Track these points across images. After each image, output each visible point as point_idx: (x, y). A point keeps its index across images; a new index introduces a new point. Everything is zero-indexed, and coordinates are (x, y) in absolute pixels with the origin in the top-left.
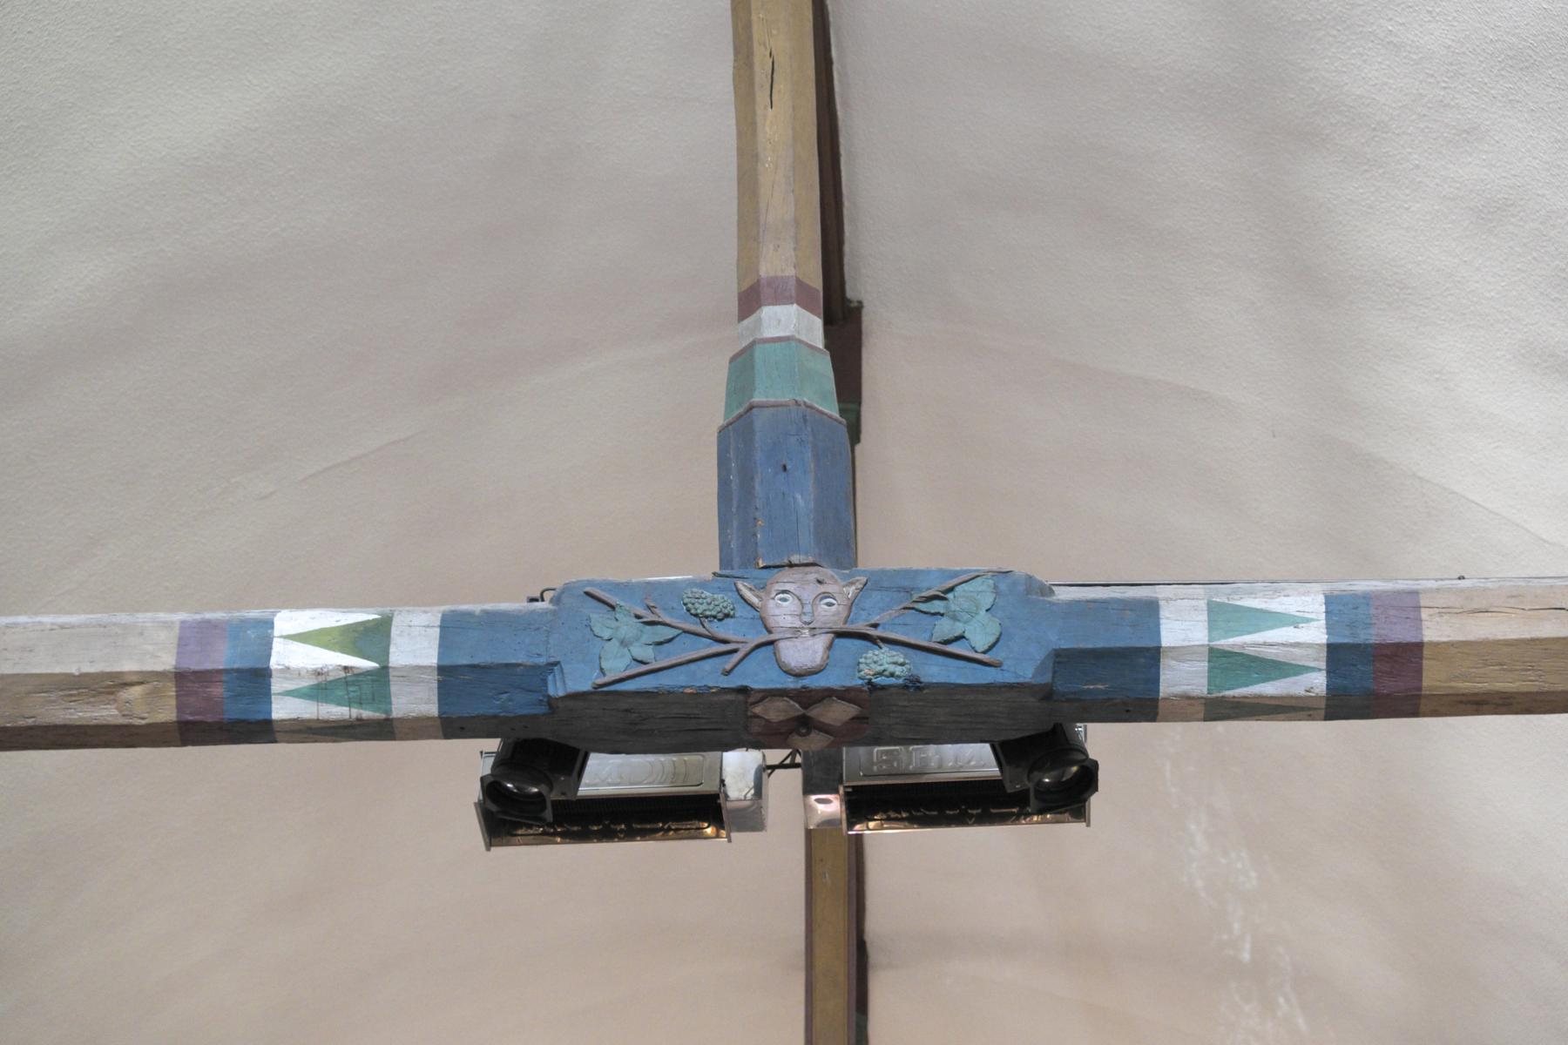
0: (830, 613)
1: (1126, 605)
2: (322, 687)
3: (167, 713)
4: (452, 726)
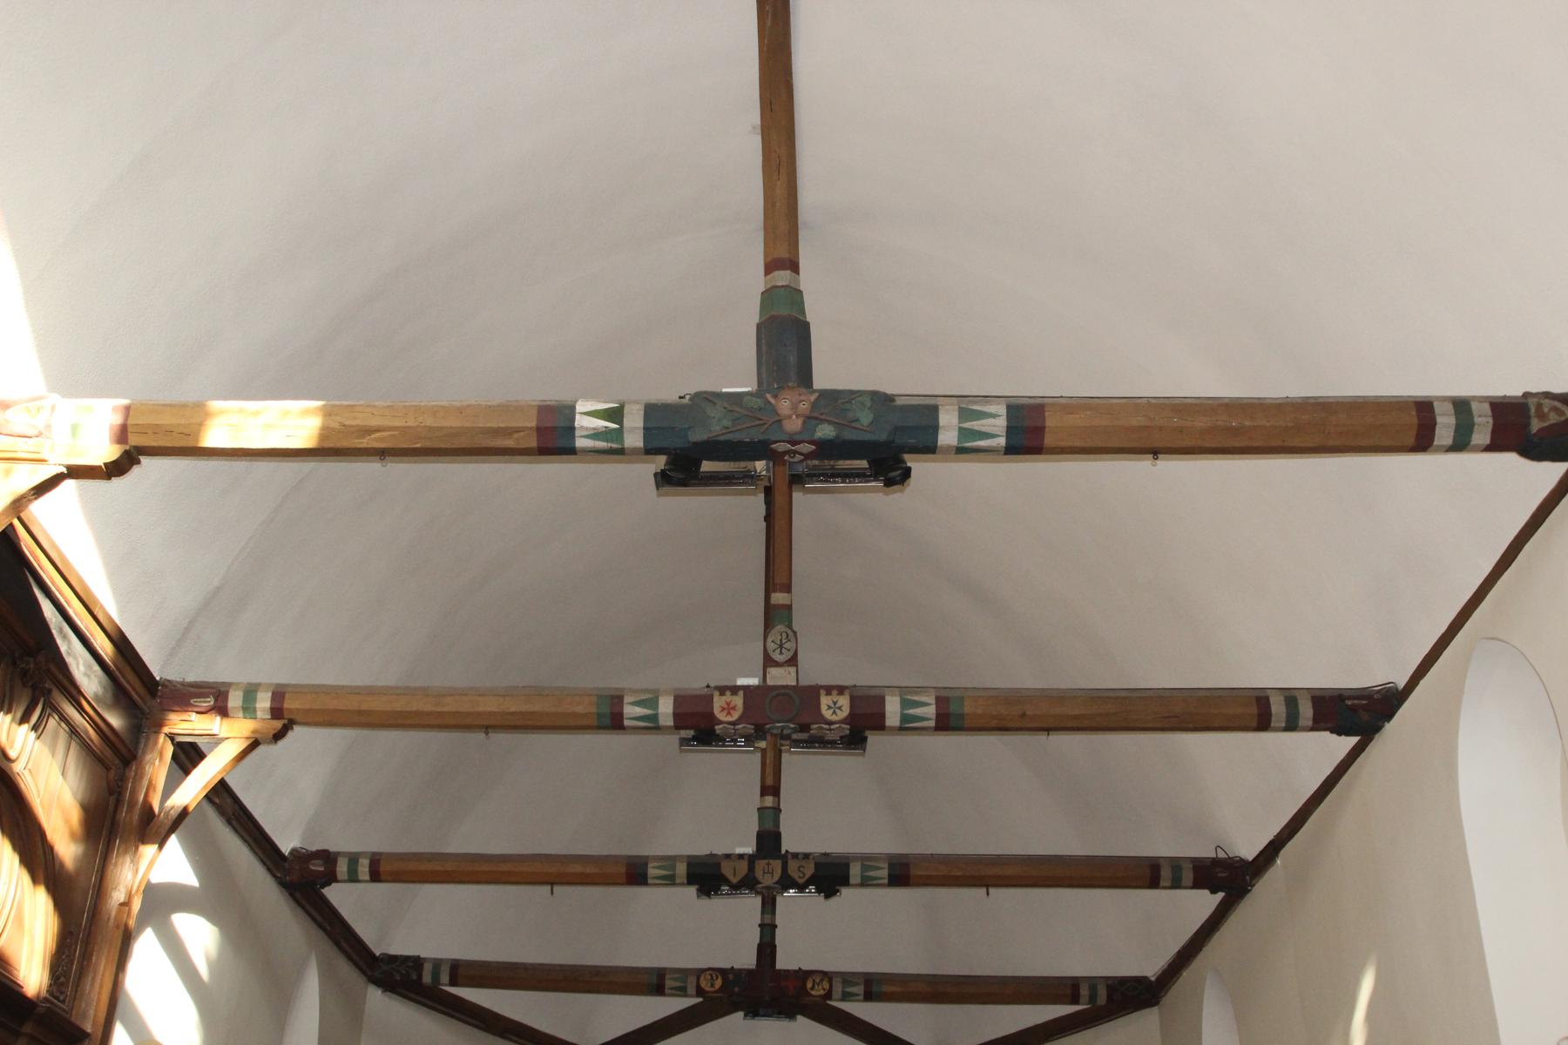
0: (804, 407)
1: (927, 407)
2: (596, 435)
3: (533, 443)
4: (649, 451)
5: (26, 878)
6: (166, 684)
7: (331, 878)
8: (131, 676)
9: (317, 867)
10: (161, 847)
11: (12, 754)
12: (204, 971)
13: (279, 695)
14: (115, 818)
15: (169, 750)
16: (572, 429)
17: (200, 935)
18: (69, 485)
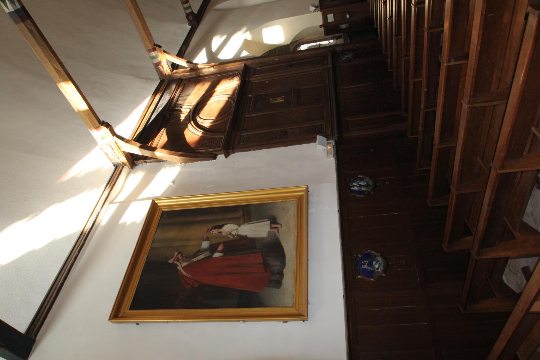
3: (28, 21)
5: (215, 94)
6: (160, 78)
7: (192, 13)
8: (161, 89)
9: (191, 17)
10: (197, 64)
11: (189, 110)
12: (224, 37)
13: (150, 51)
14: (195, 77)
15: (175, 71)
16: (15, 11)
17: (216, 41)
18: (118, 133)
